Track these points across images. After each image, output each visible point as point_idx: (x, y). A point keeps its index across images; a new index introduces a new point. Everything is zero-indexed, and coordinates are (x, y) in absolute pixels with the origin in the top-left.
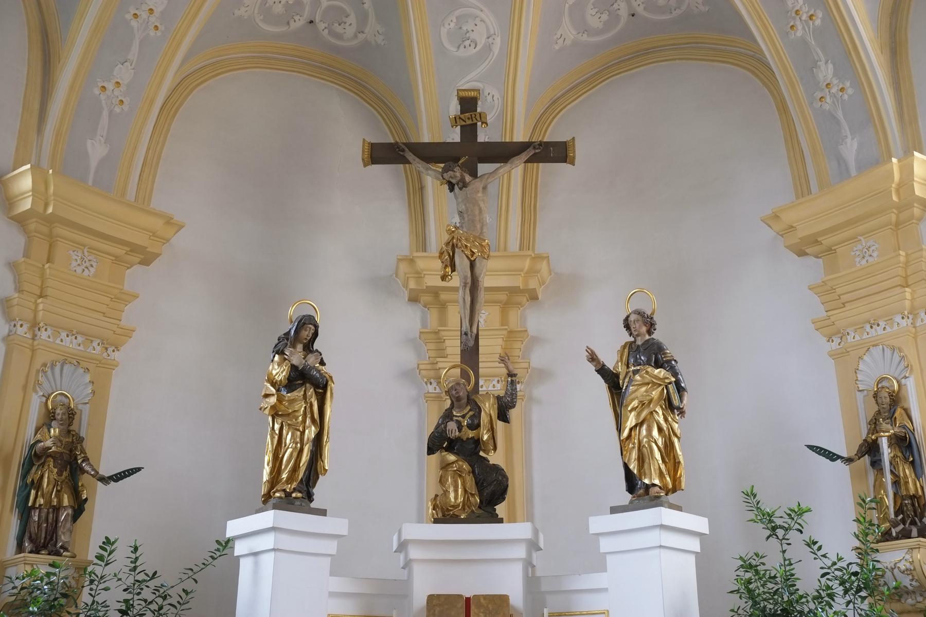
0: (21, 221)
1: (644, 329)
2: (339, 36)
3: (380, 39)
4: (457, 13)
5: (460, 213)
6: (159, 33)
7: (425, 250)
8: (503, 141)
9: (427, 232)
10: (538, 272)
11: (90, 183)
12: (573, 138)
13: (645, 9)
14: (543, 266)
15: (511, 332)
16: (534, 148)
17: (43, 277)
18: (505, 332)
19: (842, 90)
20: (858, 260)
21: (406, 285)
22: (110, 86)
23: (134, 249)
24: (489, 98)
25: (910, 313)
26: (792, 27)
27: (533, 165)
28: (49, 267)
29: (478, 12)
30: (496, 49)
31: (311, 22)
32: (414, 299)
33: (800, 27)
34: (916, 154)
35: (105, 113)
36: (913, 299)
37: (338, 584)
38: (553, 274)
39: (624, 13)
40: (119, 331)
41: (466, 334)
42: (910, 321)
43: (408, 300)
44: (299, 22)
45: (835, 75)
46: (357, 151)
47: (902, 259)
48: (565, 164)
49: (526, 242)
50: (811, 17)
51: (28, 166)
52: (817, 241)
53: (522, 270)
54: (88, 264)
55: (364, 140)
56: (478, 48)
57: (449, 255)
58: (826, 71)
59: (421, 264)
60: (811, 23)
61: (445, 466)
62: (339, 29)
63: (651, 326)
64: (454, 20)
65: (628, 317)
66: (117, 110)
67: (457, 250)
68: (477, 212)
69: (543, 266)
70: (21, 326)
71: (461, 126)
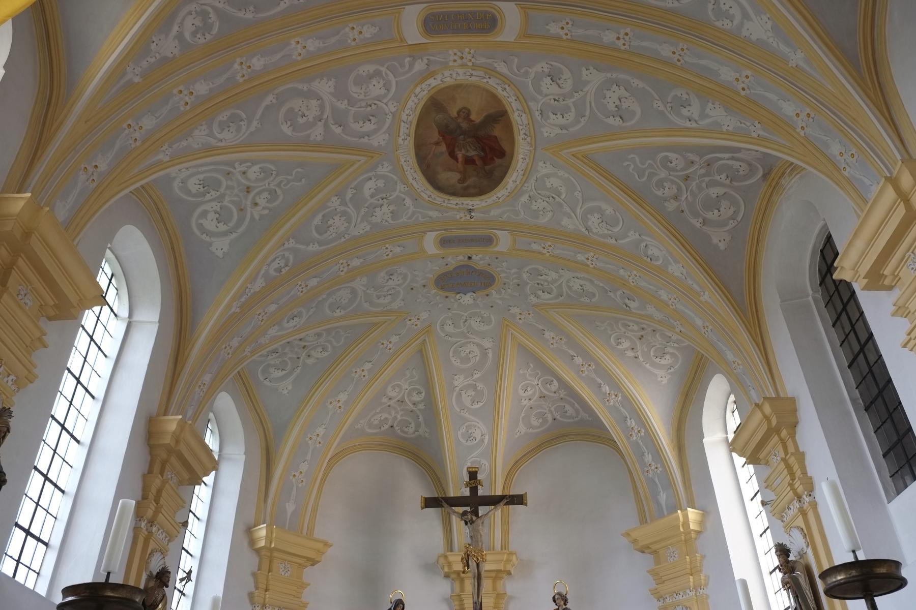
0: (258, 551)
1: (562, 603)
2: (406, 433)
3: (427, 435)
4: (466, 425)
5: (471, 537)
6: (321, 445)
7: (452, 551)
8: (493, 494)
9: (453, 538)
10: (511, 561)
11: (287, 528)
12: (526, 493)
13: (560, 417)
14: (514, 558)
15: (498, 594)
16: (507, 499)
17: (267, 580)
18: (495, 595)
19: (656, 468)
20: (669, 558)
21: (443, 568)
22: (297, 474)
23: (308, 559)
24: (483, 466)
25: (694, 588)
26: (631, 435)
27: (509, 508)
28: (271, 575)
29: (477, 424)
31: (392, 427)
32: (447, 576)
33: (634, 436)
34: (688, 509)
35: (295, 489)
36: (694, 582)
38: (519, 560)
39: (550, 418)
40: (302, 605)
41: (476, 603)
42: (694, 593)
43: (444, 576)
44: (386, 427)
45: (653, 460)
46: (418, 503)
47: (688, 560)
48: (522, 506)
49: (505, 545)
50: (639, 431)
51: (265, 525)
52: (649, 547)
53: (502, 561)
54: (287, 570)
55: (422, 496)
56: (477, 441)
57: (466, 560)
58: (649, 458)
59: (451, 559)
60: (639, 434)
62: (406, 430)
63: (566, 602)
64: (465, 428)
65: (554, 596)
66: (300, 485)
67: (470, 557)
68: (479, 537)
69: (514, 558)
70: (258, 607)
71: (470, 488)
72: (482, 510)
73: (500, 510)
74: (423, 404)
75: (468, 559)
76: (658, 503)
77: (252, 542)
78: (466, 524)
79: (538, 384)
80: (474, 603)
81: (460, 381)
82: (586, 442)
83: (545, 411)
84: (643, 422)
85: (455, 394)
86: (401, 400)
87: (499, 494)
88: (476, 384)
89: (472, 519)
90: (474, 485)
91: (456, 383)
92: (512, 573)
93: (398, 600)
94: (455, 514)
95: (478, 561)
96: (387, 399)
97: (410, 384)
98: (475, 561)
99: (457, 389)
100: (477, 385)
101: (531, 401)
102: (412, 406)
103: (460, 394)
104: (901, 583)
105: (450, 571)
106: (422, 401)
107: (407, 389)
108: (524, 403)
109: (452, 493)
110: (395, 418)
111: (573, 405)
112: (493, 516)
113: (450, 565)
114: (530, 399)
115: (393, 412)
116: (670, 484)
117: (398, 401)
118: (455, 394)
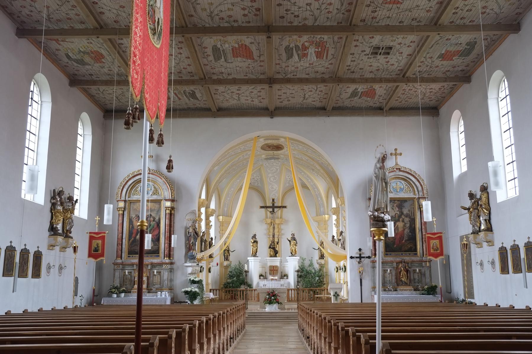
0: (220, 222)
30: (277, 189)
37: (260, 264)
58: (319, 199)
61: (271, 250)
63: (294, 235)
72: (276, 210)
76: (321, 210)
77: (218, 220)
80: (273, 234)
81: (270, 175)
84: (318, 190)
109: (268, 205)
112: (278, 212)
116: (324, 207)
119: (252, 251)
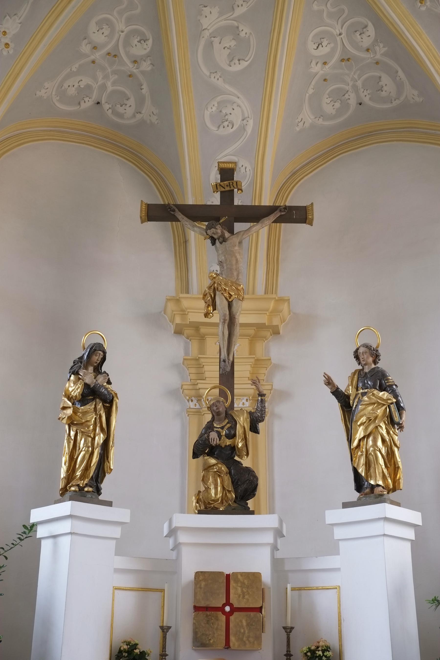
3: (154, 119)
7: (188, 292)
9: (190, 278)
13: (370, 99)
14: (285, 307)
15: (257, 360)
16: (281, 211)
18: (253, 360)
21: (172, 320)
24: (243, 170)
29: (236, 99)
30: (249, 129)
31: (98, 103)
32: (178, 332)
38: (291, 313)
39: (353, 102)
44: (88, 103)
55: (142, 201)
61: (207, 468)
62: (120, 110)
63: (376, 357)
64: (216, 105)
65: (358, 349)
67: (217, 293)
68: (234, 262)
69: (285, 307)
73: (266, 229)
74: (149, 62)
75: (215, 296)
78: (213, 243)
79: (340, 34)
80: (222, 361)
82: (401, 142)
83: (347, 88)
85: (202, 42)
86: (113, 54)
87: (267, 204)
88: (238, 27)
89: (223, 236)
90: (228, 189)
91: (205, 23)
92: (281, 332)
93: (95, 344)
94: (195, 229)
95: (230, 298)
96: (89, 47)
97: (129, 21)
98: (226, 298)
99: (207, 34)
100: (240, 29)
101: (327, 67)
102: (131, 65)
103: (210, 44)
104: (343, 503)
105: (184, 323)
106: (148, 56)
107: (122, 32)
108: (316, 68)
110: (103, 87)
111: (393, 75)
113: (184, 313)
114: (325, 63)
115: (100, 75)
117: (109, 54)
118: (202, 42)
119: (65, 459)
